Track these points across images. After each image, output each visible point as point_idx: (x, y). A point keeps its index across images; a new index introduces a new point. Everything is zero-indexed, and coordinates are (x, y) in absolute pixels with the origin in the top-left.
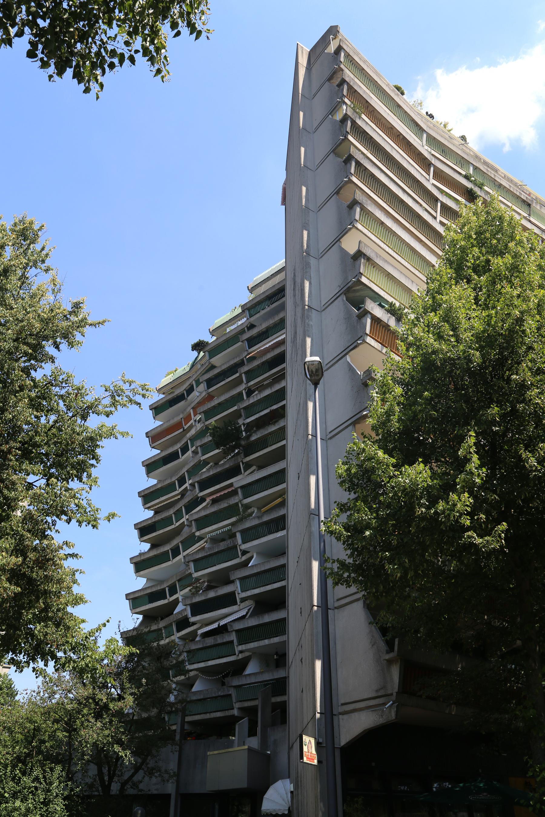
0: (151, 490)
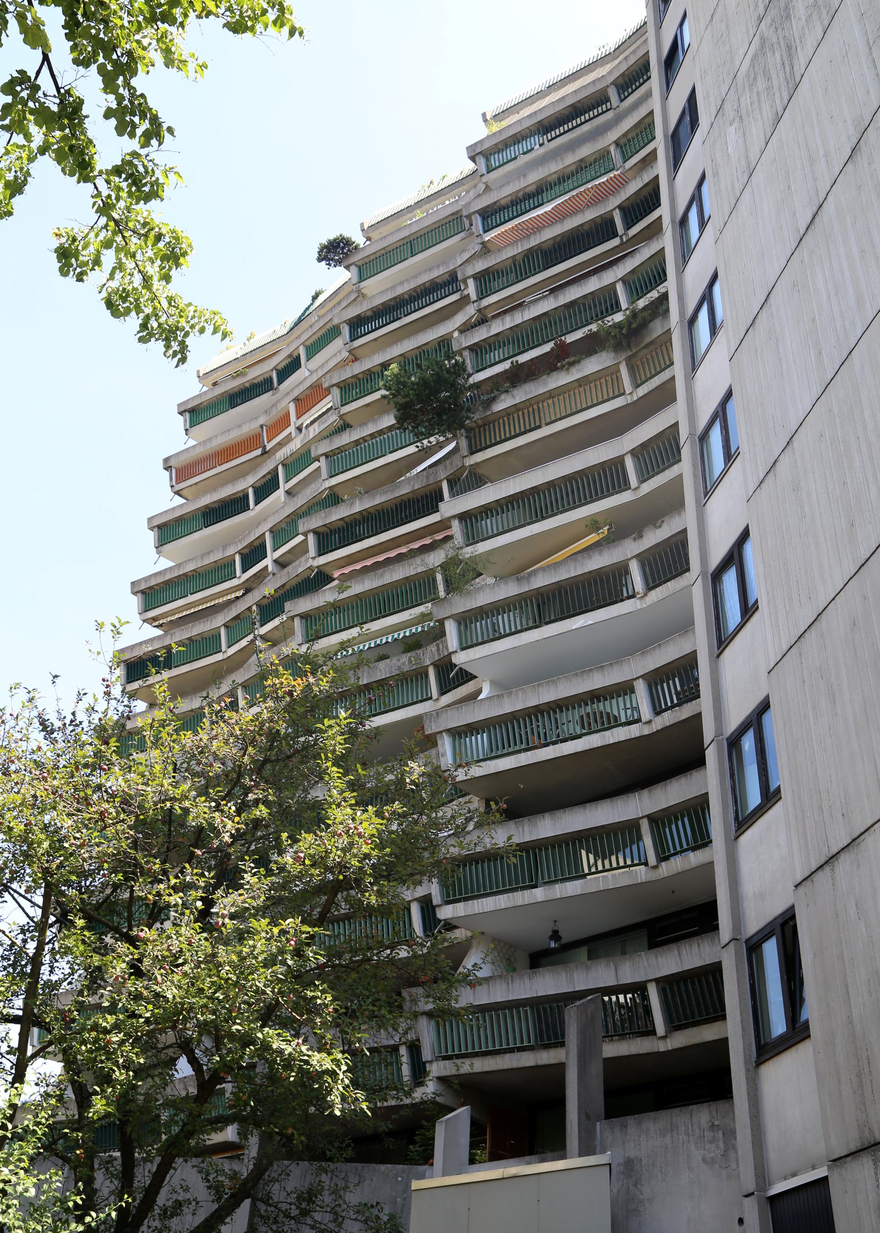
0: (168, 577)
